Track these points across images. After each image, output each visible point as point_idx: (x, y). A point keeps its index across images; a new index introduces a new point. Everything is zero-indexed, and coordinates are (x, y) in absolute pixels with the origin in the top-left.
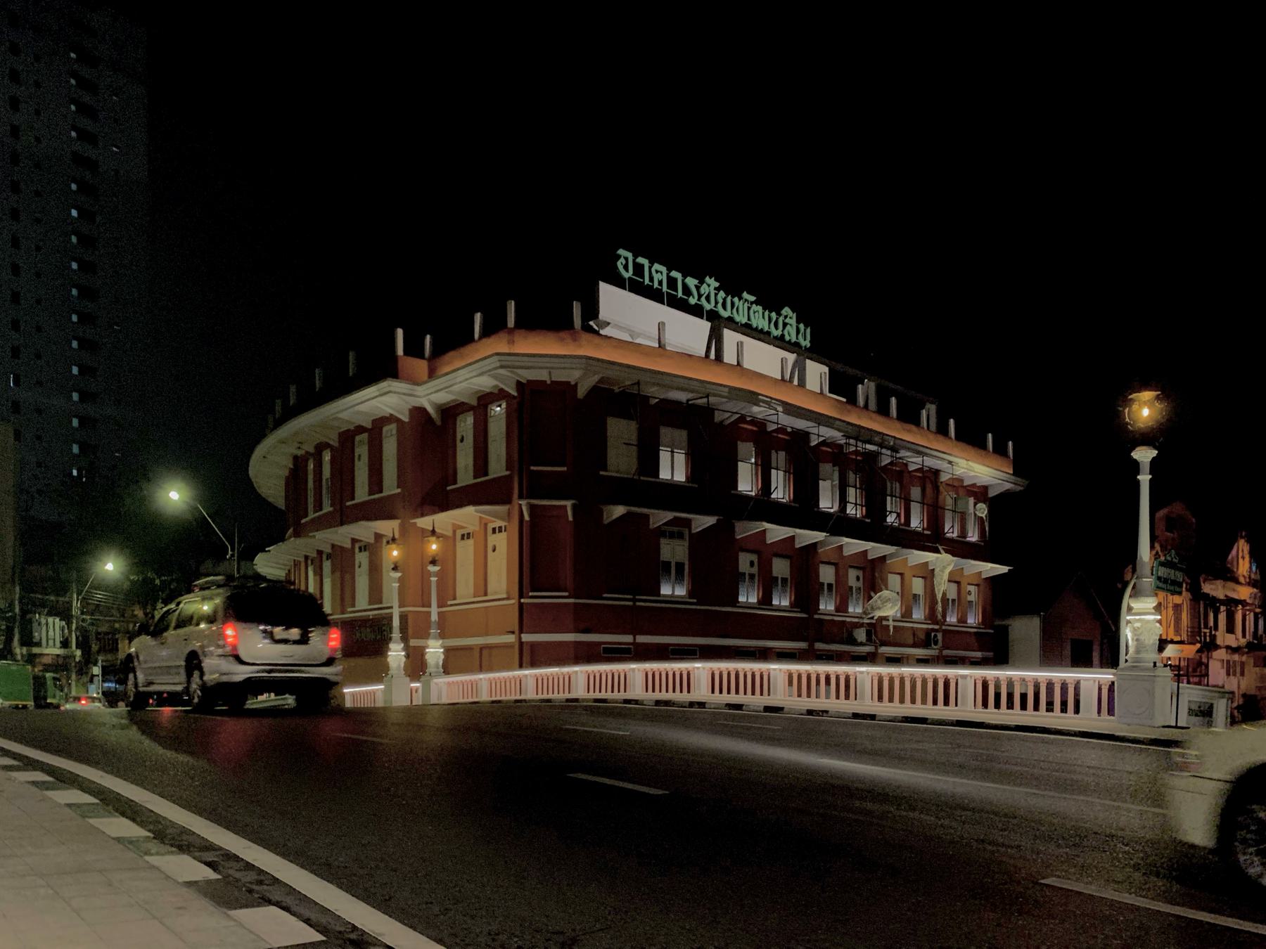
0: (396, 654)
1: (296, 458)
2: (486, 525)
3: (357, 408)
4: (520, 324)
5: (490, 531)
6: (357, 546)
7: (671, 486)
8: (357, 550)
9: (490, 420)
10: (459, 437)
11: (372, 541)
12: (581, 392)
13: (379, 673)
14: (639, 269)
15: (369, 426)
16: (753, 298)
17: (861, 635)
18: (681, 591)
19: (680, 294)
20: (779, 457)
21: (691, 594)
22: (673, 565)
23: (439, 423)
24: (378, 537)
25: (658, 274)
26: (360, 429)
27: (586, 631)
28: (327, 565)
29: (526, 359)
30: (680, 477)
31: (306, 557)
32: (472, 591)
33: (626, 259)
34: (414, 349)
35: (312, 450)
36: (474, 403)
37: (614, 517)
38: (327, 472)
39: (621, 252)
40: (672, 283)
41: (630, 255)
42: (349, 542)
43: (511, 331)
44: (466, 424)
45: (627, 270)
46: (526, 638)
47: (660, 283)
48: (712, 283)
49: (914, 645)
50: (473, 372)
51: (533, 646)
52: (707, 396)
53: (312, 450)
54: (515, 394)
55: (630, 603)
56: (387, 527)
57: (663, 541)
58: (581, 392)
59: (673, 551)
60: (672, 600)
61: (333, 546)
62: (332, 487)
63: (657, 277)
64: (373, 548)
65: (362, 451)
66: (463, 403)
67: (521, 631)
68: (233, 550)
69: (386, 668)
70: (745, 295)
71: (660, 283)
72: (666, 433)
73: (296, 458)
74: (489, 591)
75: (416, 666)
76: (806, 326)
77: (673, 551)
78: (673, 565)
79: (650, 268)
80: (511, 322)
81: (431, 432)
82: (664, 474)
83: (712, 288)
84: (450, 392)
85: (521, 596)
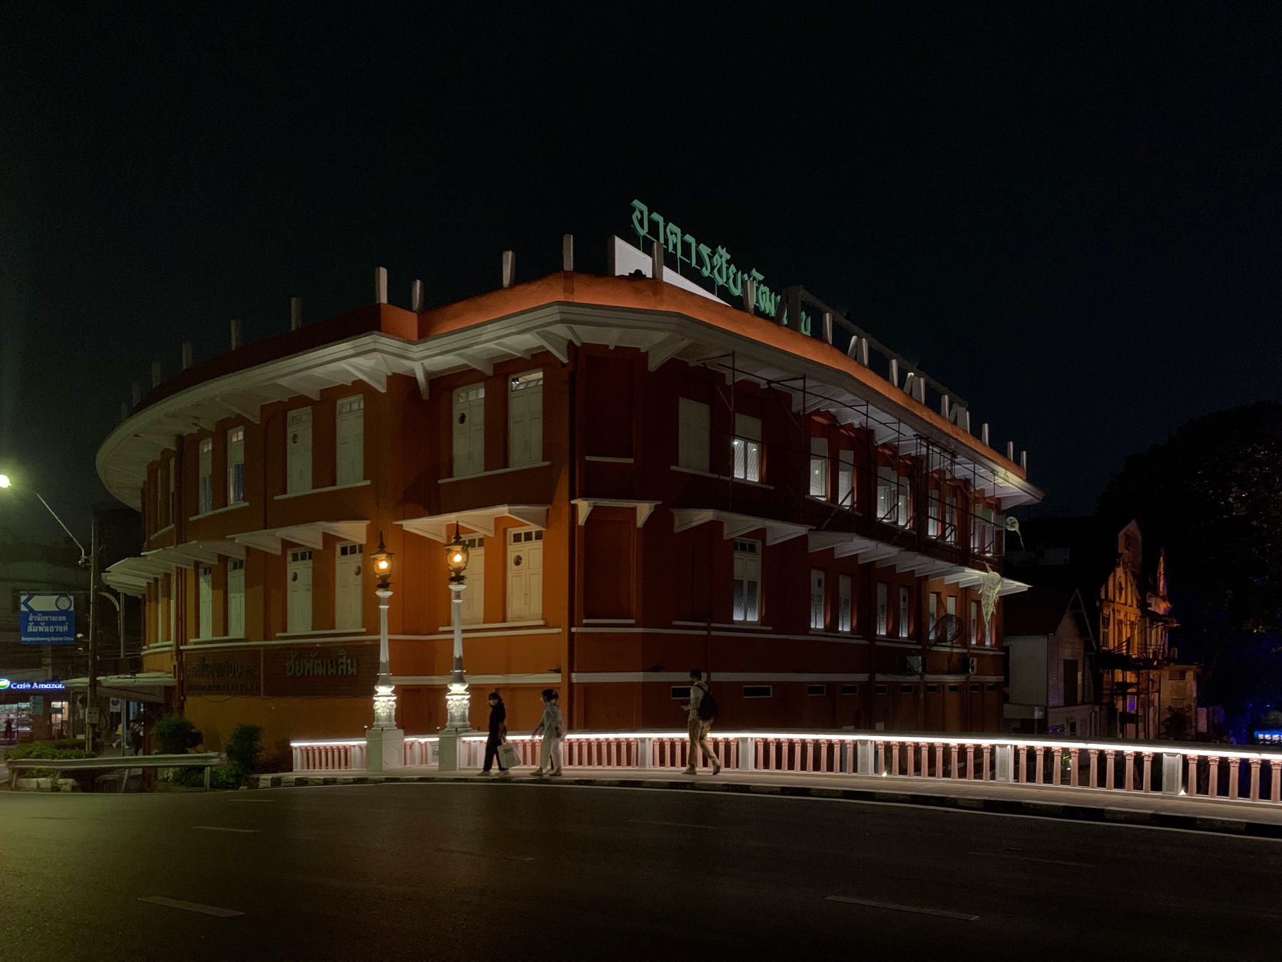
0: (384, 700)
1: (180, 439)
2: (505, 530)
3: (311, 372)
4: (518, 279)
5: (510, 538)
6: (290, 553)
7: (744, 486)
8: (289, 558)
9: (511, 395)
10: (456, 417)
11: (320, 547)
12: (654, 364)
13: (359, 720)
14: (654, 227)
15: (317, 398)
16: (761, 277)
17: (916, 662)
18: (753, 617)
19: (694, 264)
20: (847, 456)
21: (764, 620)
22: (745, 586)
23: (426, 396)
24: (329, 540)
25: (673, 235)
26: (300, 401)
27: (655, 669)
28: (237, 579)
29: (630, 315)
30: (753, 477)
31: (197, 565)
32: (480, 612)
33: (642, 213)
34: (400, 297)
35: (210, 426)
36: (490, 372)
37: (694, 524)
38: (237, 456)
39: (636, 203)
40: (686, 247)
41: (645, 208)
42: (279, 546)
43: (568, 276)
44: (472, 399)
45: (642, 227)
46: (576, 678)
47: (675, 246)
48: (723, 254)
49: (949, 673)
50: (509, 327)
51: (588, 688)
52: (804, 378)
53: (210, 426)
54: (565, 361)
55: (705, 633)
56: (355, 531)
57: (737, 555)
58: (654, 364)
59: (747, 567)
60: (745, 627)
61: (248, 549)
62: (267, 471)
63: (671, 239)
64: (322, 561)
65: (301, 429)
66: (474, 370)
67: (571, 670)
68: (88, 553)
69: (370, 714)
70: (754, 272)
71: (675, 246)
72: (741, 421)
73: (180, 439)
74: (509, 615)
75: (421, 711)
76: (807, 316)
77: (747, 567)
78: (745, 586)
79: (665, 227)
80: (569, 264)
81: (416, 412)
82: (739, 474)
83: (724, 260)
84: (461, 355)
85: (571, 624)
